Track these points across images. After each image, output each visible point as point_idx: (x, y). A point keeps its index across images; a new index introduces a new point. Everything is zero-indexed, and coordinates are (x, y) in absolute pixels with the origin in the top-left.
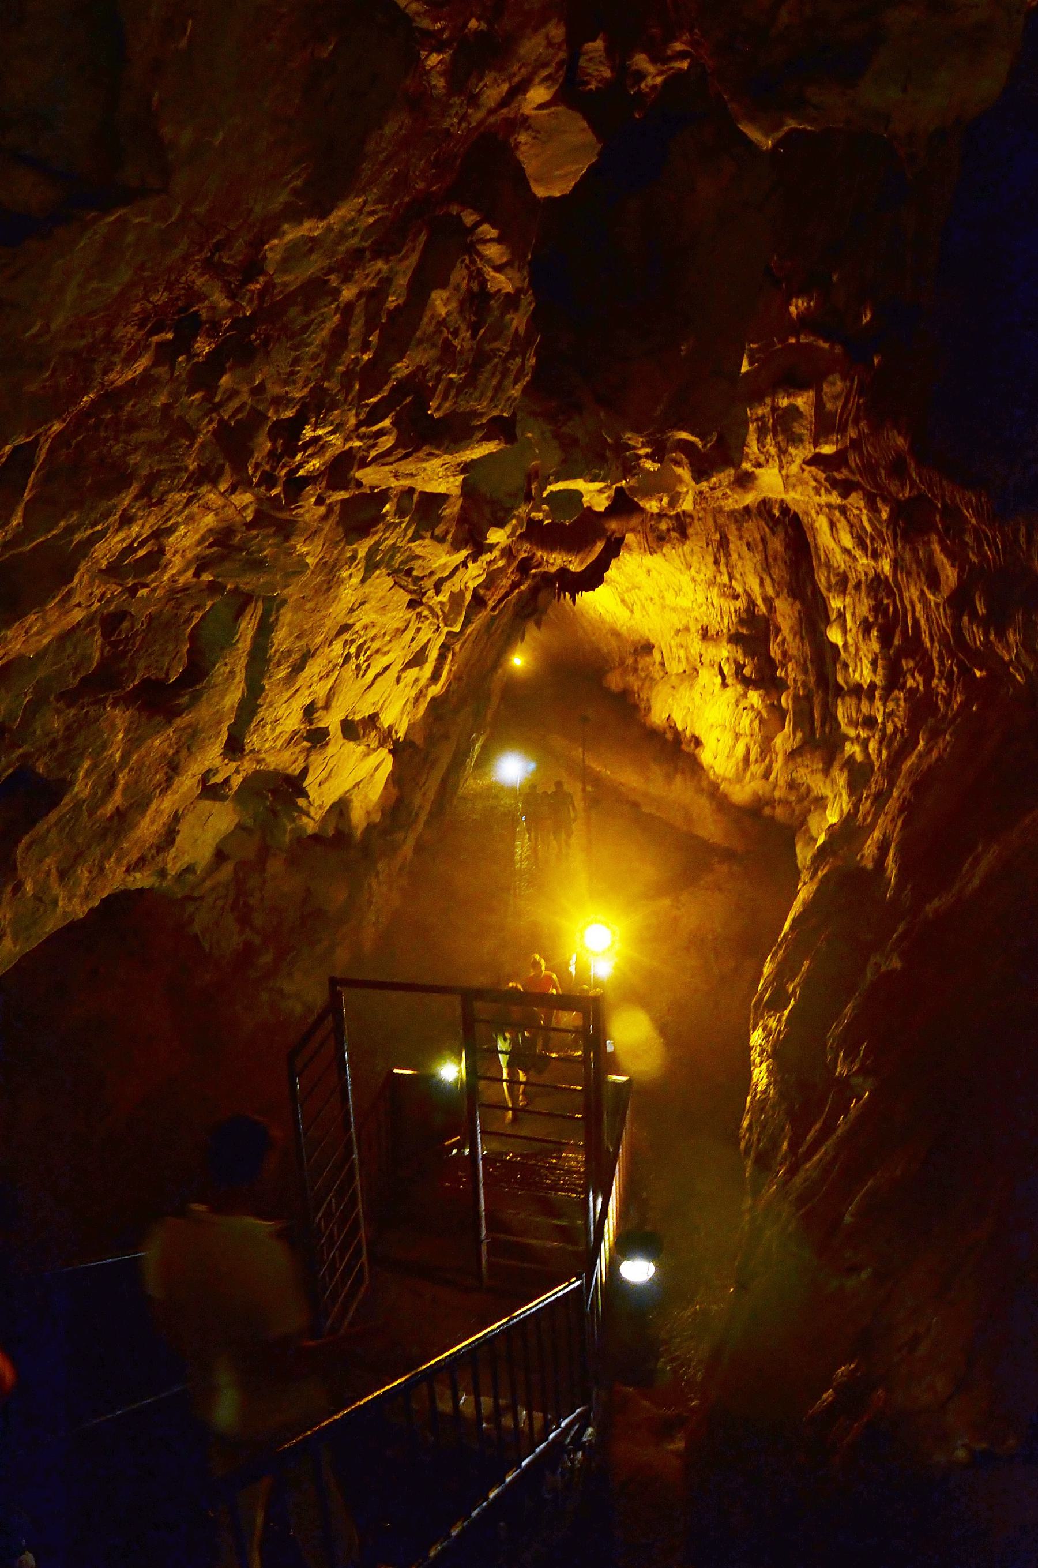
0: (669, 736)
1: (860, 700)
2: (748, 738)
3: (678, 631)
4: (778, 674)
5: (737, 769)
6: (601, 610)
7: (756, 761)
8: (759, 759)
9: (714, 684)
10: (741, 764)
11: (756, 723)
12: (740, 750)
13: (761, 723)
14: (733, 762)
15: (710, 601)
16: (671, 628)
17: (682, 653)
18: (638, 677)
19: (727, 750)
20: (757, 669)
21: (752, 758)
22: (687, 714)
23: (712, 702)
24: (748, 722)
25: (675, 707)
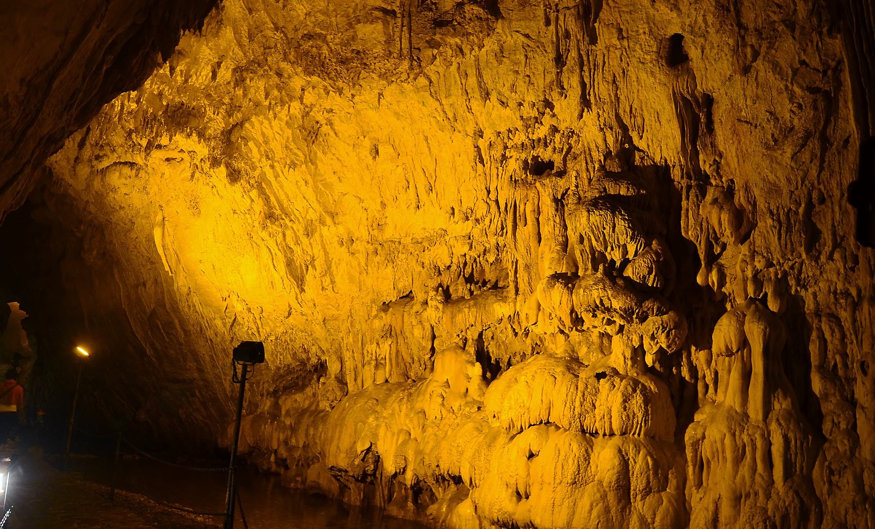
0: (354, 496)
1: (444, 521)
2: (617, 440)
3: (386, 307)
4: (699, 280)
5: (607, 510)
6: (239, 307)
7: (647, 491)
8: (653, 483)
9: (469, 378)
10: (611, 498)
11: (637, 400)
12: (605, 459)
13: (646, 402)
14: (587, 497)
15: (493, 196)
16: (373, 301)
17: (386, 349)
18: (282, 427)
19: (571, 468)
20: (661, 268)
21: (637, 483)
22: (405, 443)
23: (518, 366)
24: (619, 399)
25: (382, 432)
